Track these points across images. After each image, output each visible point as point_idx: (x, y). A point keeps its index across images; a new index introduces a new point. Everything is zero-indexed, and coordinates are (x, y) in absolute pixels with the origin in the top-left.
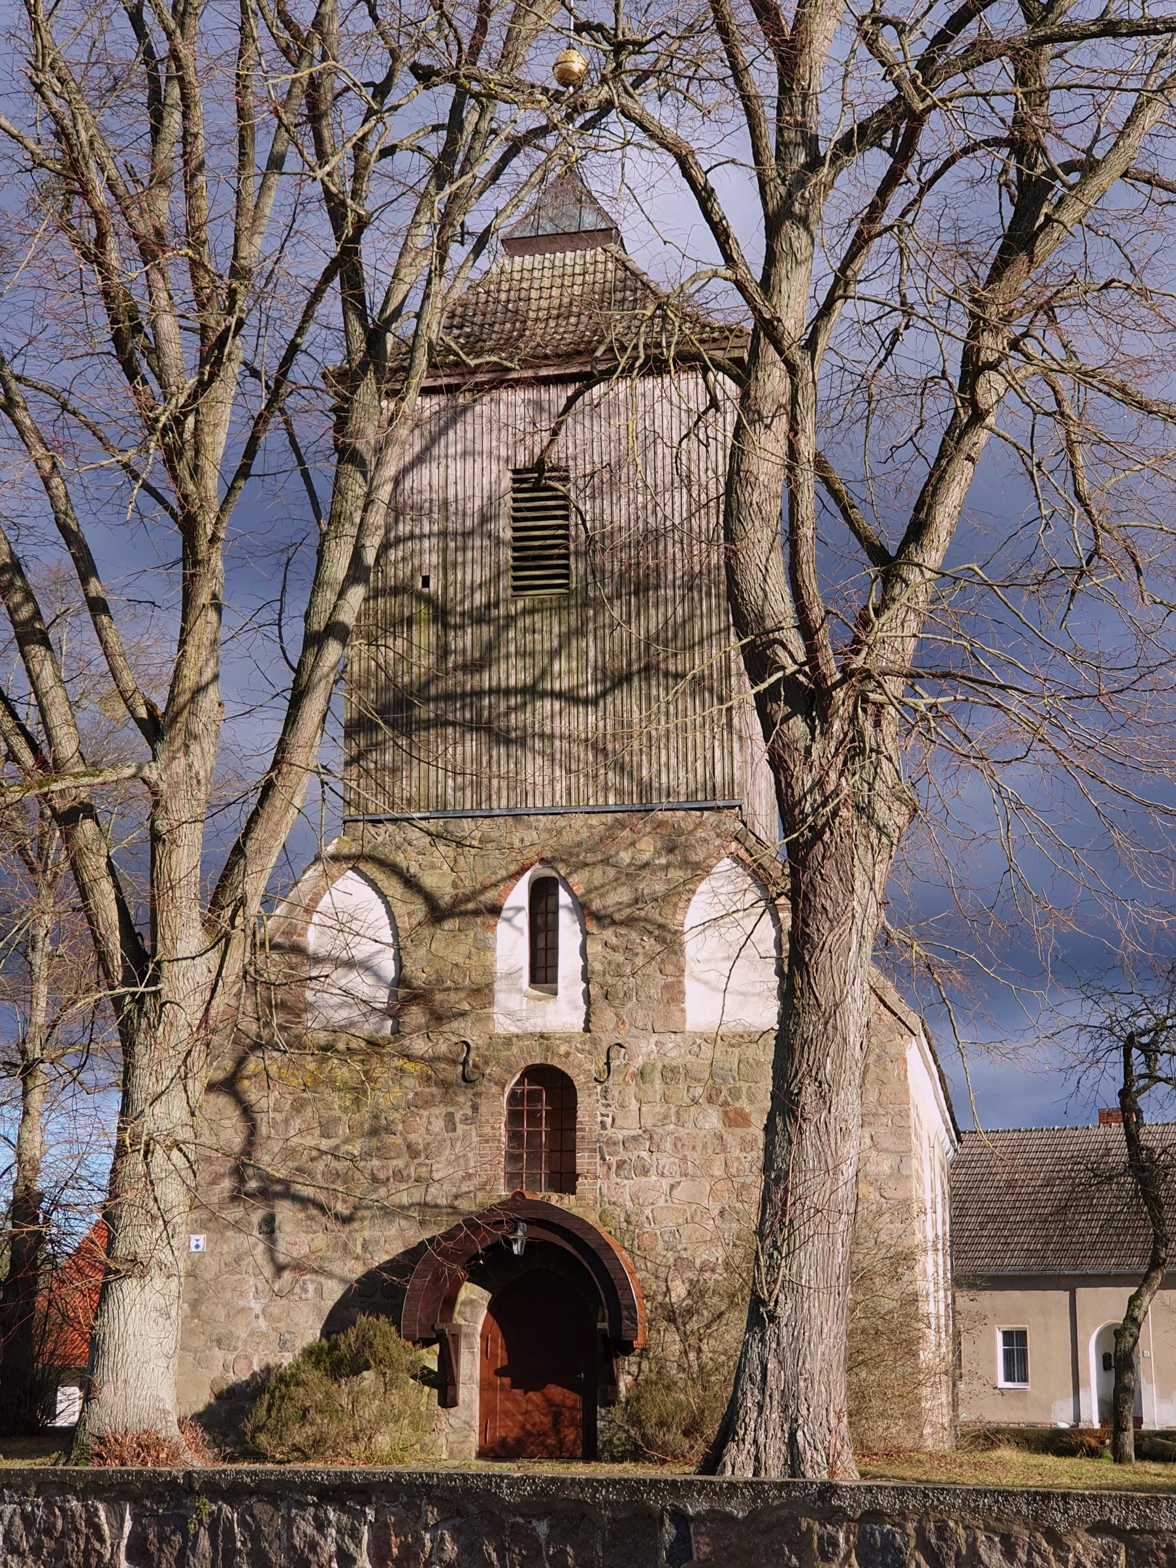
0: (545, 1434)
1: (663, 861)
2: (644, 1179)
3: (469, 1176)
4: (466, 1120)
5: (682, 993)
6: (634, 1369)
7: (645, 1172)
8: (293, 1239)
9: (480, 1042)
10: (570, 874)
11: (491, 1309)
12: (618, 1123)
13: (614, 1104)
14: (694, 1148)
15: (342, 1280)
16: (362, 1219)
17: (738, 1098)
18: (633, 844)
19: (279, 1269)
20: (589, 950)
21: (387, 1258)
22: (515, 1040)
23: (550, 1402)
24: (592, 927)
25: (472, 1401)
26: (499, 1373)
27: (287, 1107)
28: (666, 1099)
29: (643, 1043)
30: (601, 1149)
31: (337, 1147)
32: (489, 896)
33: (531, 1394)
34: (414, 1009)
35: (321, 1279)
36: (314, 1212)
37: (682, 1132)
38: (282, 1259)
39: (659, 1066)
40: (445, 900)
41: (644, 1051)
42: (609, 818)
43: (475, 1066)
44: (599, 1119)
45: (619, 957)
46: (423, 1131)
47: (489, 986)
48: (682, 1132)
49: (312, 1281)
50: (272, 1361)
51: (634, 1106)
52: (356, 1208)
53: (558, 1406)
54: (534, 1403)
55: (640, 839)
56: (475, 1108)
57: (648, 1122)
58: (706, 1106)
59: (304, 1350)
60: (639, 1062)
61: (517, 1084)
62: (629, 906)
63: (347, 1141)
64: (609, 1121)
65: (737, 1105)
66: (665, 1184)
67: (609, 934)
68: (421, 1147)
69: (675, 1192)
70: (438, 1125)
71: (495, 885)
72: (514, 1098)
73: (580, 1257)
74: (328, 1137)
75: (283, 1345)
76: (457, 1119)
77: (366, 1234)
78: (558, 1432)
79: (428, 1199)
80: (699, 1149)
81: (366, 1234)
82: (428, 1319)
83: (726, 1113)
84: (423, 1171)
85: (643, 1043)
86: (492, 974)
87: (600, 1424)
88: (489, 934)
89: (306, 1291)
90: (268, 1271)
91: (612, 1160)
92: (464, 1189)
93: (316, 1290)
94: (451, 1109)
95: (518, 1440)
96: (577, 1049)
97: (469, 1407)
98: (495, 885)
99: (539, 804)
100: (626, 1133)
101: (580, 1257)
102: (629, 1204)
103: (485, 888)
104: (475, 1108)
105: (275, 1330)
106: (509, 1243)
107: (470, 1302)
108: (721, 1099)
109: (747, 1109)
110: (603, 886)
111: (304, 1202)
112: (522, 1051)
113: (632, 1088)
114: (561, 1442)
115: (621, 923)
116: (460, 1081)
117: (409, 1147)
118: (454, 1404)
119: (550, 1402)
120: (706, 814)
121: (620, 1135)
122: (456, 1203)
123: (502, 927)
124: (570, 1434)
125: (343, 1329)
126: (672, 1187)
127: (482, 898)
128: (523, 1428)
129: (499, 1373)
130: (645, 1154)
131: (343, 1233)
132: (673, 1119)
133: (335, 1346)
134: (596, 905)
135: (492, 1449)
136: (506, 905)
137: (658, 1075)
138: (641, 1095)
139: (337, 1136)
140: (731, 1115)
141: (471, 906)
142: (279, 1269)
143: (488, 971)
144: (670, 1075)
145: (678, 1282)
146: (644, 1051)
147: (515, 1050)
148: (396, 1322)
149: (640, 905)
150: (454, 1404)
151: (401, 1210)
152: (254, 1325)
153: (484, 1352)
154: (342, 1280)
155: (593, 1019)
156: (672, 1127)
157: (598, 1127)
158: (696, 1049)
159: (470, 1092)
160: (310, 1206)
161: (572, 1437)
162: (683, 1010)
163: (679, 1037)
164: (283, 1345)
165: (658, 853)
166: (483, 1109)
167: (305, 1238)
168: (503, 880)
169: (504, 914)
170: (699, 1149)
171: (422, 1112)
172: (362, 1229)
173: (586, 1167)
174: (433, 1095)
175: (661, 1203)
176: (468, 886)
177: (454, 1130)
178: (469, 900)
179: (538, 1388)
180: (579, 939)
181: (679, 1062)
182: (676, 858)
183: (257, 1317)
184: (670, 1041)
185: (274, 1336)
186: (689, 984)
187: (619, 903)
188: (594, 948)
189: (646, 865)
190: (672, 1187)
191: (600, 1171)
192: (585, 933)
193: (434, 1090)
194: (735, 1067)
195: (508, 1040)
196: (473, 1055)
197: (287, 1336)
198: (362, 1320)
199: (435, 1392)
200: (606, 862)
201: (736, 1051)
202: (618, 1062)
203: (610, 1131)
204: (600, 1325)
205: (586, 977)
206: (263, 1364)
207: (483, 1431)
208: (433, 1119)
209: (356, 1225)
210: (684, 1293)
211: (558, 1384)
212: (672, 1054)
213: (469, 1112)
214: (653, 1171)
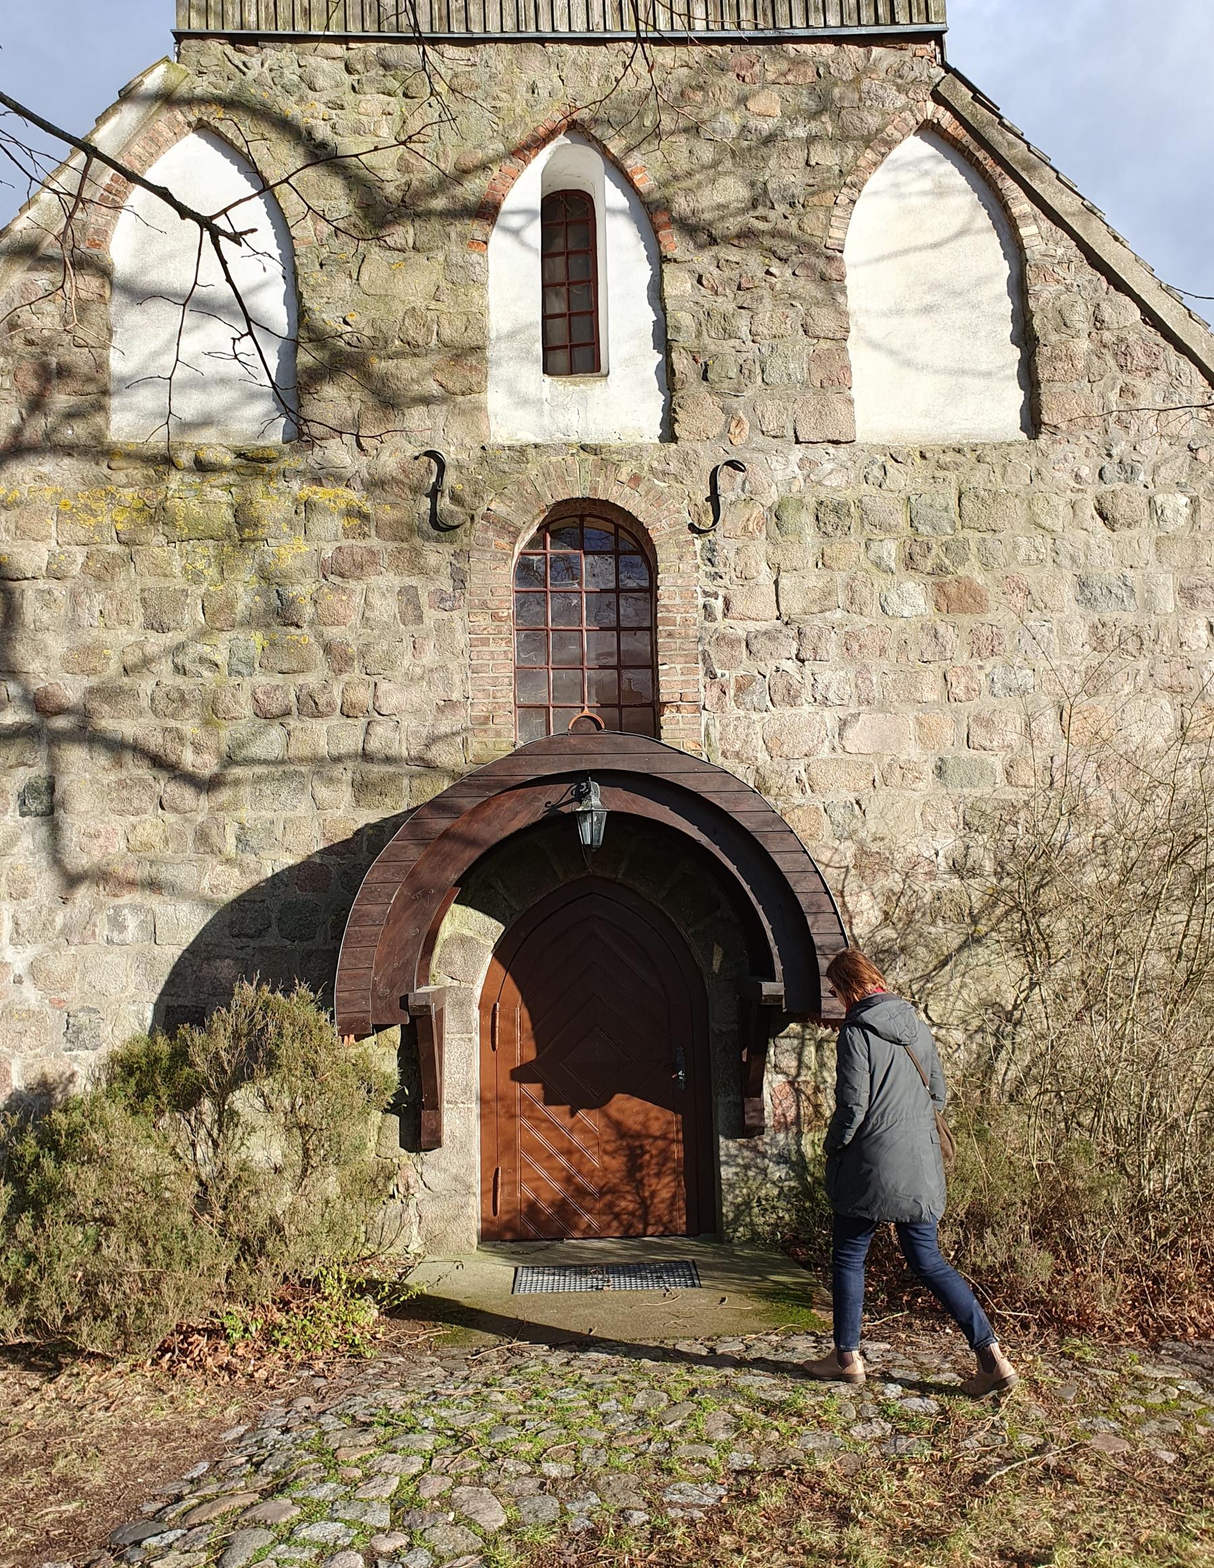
0: (613, 1191)
1: (801, 132)
2: (788, 711)
3: (449, 704)
4: (441, 600)
5: (847, 368)
6: (789, 1063)
7: (791, 697)
8: (93, 825)
9: (463, 456)
10: (630, 149)
11: (500, 952)
12: (738, 606)
13: (729, 574)
14: (883, 651)
15: (208, 903)
16: (237, 782)
17: (964, 560)
18: (743, 100)
19: (72, 881)
20: (669, 290)
21: (290, 860)
22: (531, 452)
23: (620, 1130)
24: (675, 244)
25: (469, 1135)
26: (521, 1074)
27: (76, 570)
28: (823, 561)
29: (776, 463)
30: (706, 657)
31: (180, 648)
32: (473, 188)
33: (581, 1113)
34: (329, 390)
35: (154, 902)
36: (143, 771)
37: (860, 622)
38: (79, 860)
39: (811, 501)
40: (392, 182)
41: (779, 476)
42: (697, 52)
43: (456, 499)
44: (701, 601)
45: (725, 304)
46: (355, 619)
47: (478, 349)
48: (860, 622)
49: (136, 909)
50: (53, 1068)
51: (765, 577)
52: (230, 760)
53: (638, 1136)
54: (585, 1130)
55: (754, 94)
56: (460, 580)
57: (793, 604)
58: (901, 574)
59: (114, 1059)
60: (772, 496)
61: (532, 543)
62: (744, 211)
63: (203, 634)
64: (719, 605)
65: (961, 572)
66: (830, 717)
67: (703, 261)
68: (353, 650)
69: (849, 733)
70: (386, 607)
71: (484, 167)
72: (525, 570)
73: (716, 850)
74: (162, 629)
75: (74, 1035)
76: (424, 599)
77: (246, 814)
78: (640, 1185)
79: (374, 745)
80: (892, 653)
81: (246, 814)
82: (392, 985)
83: (940, 587)
84: (362, 695)
85: (776, 463)
86: (482, 330)
87: (726, 1172)
88: (475, 257)
89: (122, 928)
90: (45, 884)
91: (729, 676)
92: (444, 728)
93: (142, 925)
94: (413, 581)
95: (561, 1206)
96: (652, 469)
97: (464, 1148)
98: (484, 167)
99: (562, 28)
100: (752, 626)
101: (716, 850)
102: (763, 756)
103: (463, 173)
104: (460, 580)
105: (58, 1004)
106: (575, 819)
107: (463, 941)
108: (929, 564)
109: (979, 579)
110: (689, 174)
111: (117, 747)
112: (546, 475)
113: (759, 548)
114: (645, 1205)
115: (727, 240)
116: (427, 526)
117: (327, 649)
118: (436, 1143)
119: (620, 1130)
120: (876, 51)
121: (741, 630)
122: (429, 755)
123: (497, 239)
124: (664, 1188)
125: (199, 1018)
126: (844, 724)
127: (458, 191)
128: (569, 1180)
129: (521, 1074)
130: (791, 666)
131: (200, 806)
132: (842, 598)
133: (181, 1056)
134: (682, 205)
135: (508, 1226)
136: (505, 206)
137: (807, 518)
138: (778, 558)
139: (179, 627)
140: (952, 590)
141: (439, 203)
142: (72, 881)
143: (475, 319)
144: (832, 518)
145: (865, 897)
146: (779, 476)
147: (532, 470)
148: (325, 1003)
149: (761, 211)
150: (436, 1143)
151: (323, 765)
152: (13, 996)
153: (490, 1034)
154: (208, 903)
155: (681, 415)
156: (839, 614)
157: (698, 615)
158: (877, 472)
159: (447, 549)
160: (128, 757)
161: (665, 1194)
162: (851, 401)
163: (842, 452)
164: (74, 1035)
165: (791, 117)
166: (474, 581)
167: (119, 824)
168: (497, 159)
169: (501, 220)
170: (892, 653)
171: (352, 584)
172: (235, 804)
173: (678, 689)
174: (372, 553)
175: (824, 752)
176: (425, 172)
177: (419, 619)
178: (433, 194)
179: (598, 1102)
180: (645, 273)
181: (849, 495)
182: (827, 124)
183: (19, 981)
184: (829, 461)
185: (55, 1019)
186: (857, 353)
187: (720, 207)
188: (678, 285)
189: (769, 140)
190: (844, 724)
191: (708, 696)
192: (659, 260)
193: (375, 542)
194: (953, 502)
195: (520, 453)
196: (450, 478)
197: (83, 1018)
198: (246, 992)
199: (394, 1120)
200: (694, 130)
201: (952, 476)
202: (731, 496)
203: (721, 624)
204: (768, 988)
205: (663, 340)
206: (33, 1076)
207: (492, 1189)
208: (375, 599)
209: (224, 795)
210: (875, 916)
211: (633, 1093)
212: (835, 481)
213: (447, 585)
214: (806, 695)
